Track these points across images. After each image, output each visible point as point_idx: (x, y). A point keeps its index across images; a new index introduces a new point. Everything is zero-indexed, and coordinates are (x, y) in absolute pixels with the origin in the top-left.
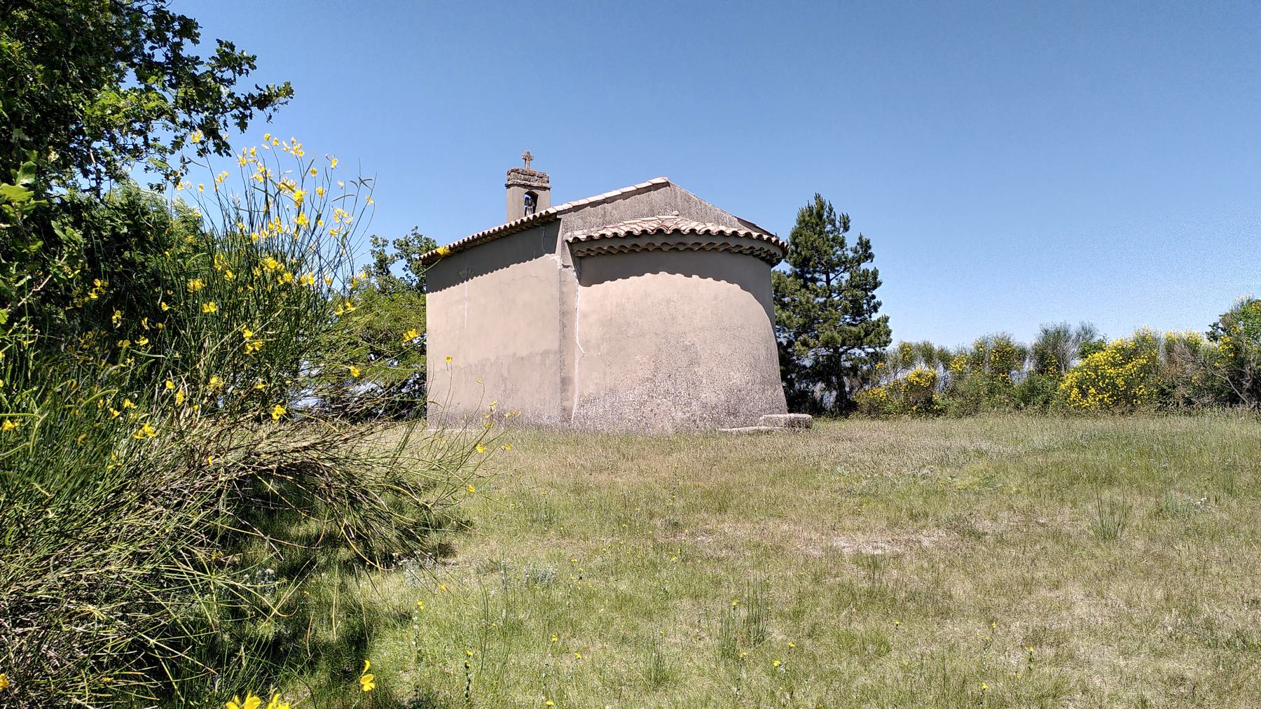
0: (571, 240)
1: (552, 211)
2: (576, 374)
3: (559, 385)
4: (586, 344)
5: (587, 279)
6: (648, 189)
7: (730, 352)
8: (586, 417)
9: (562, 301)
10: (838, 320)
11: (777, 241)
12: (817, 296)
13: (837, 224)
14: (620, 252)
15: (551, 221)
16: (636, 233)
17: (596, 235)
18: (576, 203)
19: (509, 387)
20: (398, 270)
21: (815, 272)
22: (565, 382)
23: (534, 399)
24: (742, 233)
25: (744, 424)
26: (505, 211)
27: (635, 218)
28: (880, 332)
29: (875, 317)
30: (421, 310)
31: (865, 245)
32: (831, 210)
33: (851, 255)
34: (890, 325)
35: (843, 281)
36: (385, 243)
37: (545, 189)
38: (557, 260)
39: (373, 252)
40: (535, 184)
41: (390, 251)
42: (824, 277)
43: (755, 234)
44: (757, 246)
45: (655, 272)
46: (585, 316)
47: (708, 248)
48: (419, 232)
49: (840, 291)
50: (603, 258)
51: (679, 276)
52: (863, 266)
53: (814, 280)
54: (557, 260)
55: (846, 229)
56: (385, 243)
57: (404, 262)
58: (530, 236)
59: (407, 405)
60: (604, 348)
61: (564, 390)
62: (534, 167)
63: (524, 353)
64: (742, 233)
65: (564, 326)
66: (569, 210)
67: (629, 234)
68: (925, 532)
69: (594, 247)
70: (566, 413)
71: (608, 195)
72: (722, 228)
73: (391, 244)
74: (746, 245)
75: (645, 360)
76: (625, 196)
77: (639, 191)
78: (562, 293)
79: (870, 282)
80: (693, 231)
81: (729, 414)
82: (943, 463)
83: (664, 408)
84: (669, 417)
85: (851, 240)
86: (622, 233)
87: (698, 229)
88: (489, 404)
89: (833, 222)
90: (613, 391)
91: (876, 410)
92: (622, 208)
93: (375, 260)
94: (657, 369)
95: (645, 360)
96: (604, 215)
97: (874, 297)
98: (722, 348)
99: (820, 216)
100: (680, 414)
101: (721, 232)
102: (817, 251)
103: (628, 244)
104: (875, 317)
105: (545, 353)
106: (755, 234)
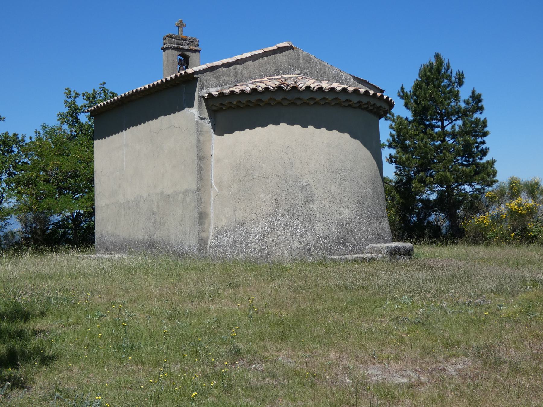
2: (212, 210)
4: (220, 184)
5: (220, 129)
6: (274, 52)
7: (340, 191)
9: (199, 148)
10: (450, 161)
11: (388, 98)
12: (433, 140)
13: (453, 79)
14: (248, 106)
15: (190, 81)
16: (260, 89)
17: (227, 92)
18: (210, 65)
19: (158, 220)
20: (84, 118)
21: (432, 119)
22: (202, 217)
23: (178, 230)
24: (362, 90)
25: (352, 252)
26: (160, 70)
27: (262, 77)
28: (486, 173)
29: (485, 160)
31: (476, 98)
32: (448, 68)
33: (463, 105)
34: (496, 166)
35: (457, 128)
36: (77, 95)
37: (195, 51)
38: (194, 113)
39: (66, 102)
41: (80, 102)
42: (439, 123)
43: (371, 92)
44: (365, 100)
45: (277, 123)
46: (218, 161)
47: (322, 102)
48: (106, 86)
49: (454, 135)
50: (234, 112)
51: (297, 127)
52: (476, 116)
53: (433, 127)
55: (460, 83)
56: (77, 95)
59: (80, 234)
60: (235, 187)
62: (186, 33)
63: (170, 192)
64: (362, 90)
65: (200, 169)
66: (205, 71)
67: (254, 90)
68: (453, 360)
69: (225, 102)
70: (203, 242)
71: (239, 57)
72: (335, 85)
73: (81, 97)
74: (355, 99)
75: (268, 198)
76: (254, 58)
77: (266, 54)
78: (199, 141)
79: (479, 130)
80: (308, 88)
81: (339, 244)
82: (499, 291)
84: (287, 245)
85: (464, 93)
86: (248, 90)
87: (312, 86)
88: (139, 234)
89: (449, 78)
90: (241, 224)
91: (480, 237)
92: (251, 68)
94: (278, 206)
95: (268, 198)
96: (236, 74)
97: (484, 143)
98: (334, 188)
99: (439, 71)
100: (297, 243)
101: (332, 89)
102: (435, 102)
104: (485, 160)
106: (371, 92)
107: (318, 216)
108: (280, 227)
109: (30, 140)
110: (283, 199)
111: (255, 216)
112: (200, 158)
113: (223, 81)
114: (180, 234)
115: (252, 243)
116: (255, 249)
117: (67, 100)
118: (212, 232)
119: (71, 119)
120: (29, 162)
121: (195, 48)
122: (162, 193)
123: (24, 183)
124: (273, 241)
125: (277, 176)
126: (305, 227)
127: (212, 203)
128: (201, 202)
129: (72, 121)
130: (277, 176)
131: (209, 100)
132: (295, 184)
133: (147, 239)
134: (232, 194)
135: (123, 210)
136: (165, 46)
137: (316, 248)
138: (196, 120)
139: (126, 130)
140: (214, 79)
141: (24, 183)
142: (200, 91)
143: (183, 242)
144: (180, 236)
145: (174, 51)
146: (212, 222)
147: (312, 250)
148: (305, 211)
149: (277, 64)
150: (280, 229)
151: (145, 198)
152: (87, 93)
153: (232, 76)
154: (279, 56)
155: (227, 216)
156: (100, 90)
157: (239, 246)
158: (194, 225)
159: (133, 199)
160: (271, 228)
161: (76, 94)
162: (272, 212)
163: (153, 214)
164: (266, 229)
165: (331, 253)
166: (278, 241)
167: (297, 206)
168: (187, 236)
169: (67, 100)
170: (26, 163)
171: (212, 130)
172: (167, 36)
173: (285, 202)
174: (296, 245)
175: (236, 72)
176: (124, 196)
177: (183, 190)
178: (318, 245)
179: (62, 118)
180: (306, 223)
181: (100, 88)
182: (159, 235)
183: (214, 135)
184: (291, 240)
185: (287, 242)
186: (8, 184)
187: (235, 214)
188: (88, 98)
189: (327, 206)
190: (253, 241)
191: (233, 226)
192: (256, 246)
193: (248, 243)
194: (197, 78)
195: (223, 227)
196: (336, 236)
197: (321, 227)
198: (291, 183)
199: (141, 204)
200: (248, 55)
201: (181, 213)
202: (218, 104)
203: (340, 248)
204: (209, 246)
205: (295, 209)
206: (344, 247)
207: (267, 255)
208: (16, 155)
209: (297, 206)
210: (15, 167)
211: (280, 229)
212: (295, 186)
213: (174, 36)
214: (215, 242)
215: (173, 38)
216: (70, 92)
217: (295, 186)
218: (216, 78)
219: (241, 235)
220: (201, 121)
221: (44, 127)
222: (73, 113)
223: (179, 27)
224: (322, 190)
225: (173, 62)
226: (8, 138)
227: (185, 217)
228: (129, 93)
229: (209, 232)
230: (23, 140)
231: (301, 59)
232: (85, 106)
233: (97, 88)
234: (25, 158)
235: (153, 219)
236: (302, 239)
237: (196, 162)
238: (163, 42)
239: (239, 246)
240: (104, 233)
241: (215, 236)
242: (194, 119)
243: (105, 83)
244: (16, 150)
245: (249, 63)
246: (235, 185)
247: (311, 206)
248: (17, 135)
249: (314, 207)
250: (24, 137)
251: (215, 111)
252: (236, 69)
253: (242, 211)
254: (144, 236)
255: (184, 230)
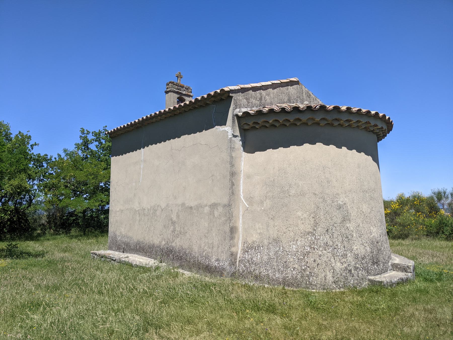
0: (240, 114)
1: (226, 89)
3: (228, 234)
4: (250, 200)
5: (250, 147)
8: (251, 261)
18: (242, 86)
19: (178, 229)
20: (93, 147)
22: (233, 230)
23: (200, 240)
30: (108, 167)
36: (88, 133)
38: (229, 129)
39: (81, 137)
40: (184, 93)
41: (90, 137)
46: (248, 177)
50: (267, 130)
51: (332, 147)
54: (229, 129)
56: (88, 133)
57: (97, 143)
58: (203, 113)
60: (268, 204)
61: (232, 238)
62: (180, 82)
71: (264, 84)
73: (91, 134)
75: (305, 215)
76: (274, 86)
81: (374, 263)
83: (324, 259)
88: (156, 239)
90: (277, 241)
93: (81, 141)
94: (316, 224)
96: (261, 99)
98: (365, 208)
100: (339, 264)
103: (291, 118)
105: (214, 206)
107: (355, 235)
108: (320, 247)
109: (55, 160)
110: (322, 217)
111: (292, 234)
112: (232, 174)
113: (252, 103)
114: (205, 246)
115: (290, 262)
116: (294, 268)
117: (82, 135)
118: (240, 246)
119: (83, 148)
120: (54, 173)
121: (189, 94)
122: (183, 204)
123: (49, 187)
124: (315, 261)
125: (315, 194)
126: (344, 247)
127: (241, 217)
128: (232, 216)
129: (84, 149)
130: (315, 194)
131: (243, 119)
132: (333, 202)
133: (165, 245)
134: (264, 210)
135: (138, 216)
136: (168, 90)
137: (356, 268)
138: (230, 137)
139: (144, 148)
140: (245, 100)
141: (49, 187)
142: (234, 110)
143: (210, 255)
144: (206, 248)
145: (175, 94)
146: (241, 236)
147: (353, 271)
148: (343, 231)
149: (289, 94)
150: (321, 249)
151: (163, 207)
152: (95, 132)
153: (258, 99)
154: (291, 89)
155: (259, 231)
156: (103, 131)
157: (275, 264)
158: (225, 239)
159: (149, 208)
160: (311, 248)
161: (88, 131)
162: (311, 230)
163: (172, 223)
164: (306, 248)
165: (369, 273)
166: (319, 261)
167: (336, 225)
168: (215, 249)
169: (82, 135)
170: (52, 174)
171: (242, 148)
172: (170, 83)
173: (323, 220)
174: (338, 266)
175: (261, 97)
176: (139, 204)
177: (209, 204)
178: (357, 266)
179: (78, 146)
180: (345, 243)
181: (104, 129)
182: (177, 244)
183: (244, 153)
184: (332, 260)
185: (329, 262)
186: (38, 187)
187: (268, 230)
188: (96, 135)
189: (361, 225)
190: (292, 260)
191: (266, 242)
192: (296, 266)
193: (286, 262)
194: (232, 97)
195: (253, 242)
196: (371, 255)
197: (358, 247)
198: (329, 201)
199: (158, 213)
200: (269, 83)
201: (206, 225)
202: (251, 123)
203: (375, 268)
204: (238, 261)
205: (334, 228)
206: (377, 266)
207: (308, 276)
208: (45, 169)
209: (336, 225)
210: (44, 176)
211: (321, 249)
212: (333, 204)
213: (175, 83)
214: (245, 258)
215: (174, 84)
216: (84, 130)
217: (333, 204)
218: (247, 99)
219: (276, 252)
220: (233, 139)
221: (65, 151)
222: (85, 143)
223: (178, 77)
224: (356, 210)
225: (174, 102)
226: (40, 157)
227: (211, 230)
228: (151, 115)
229: (238, 246)
230: (51, 159)
231: (304, 93)
232: (93, 140)
233: (101, 129)
234: (51, 171)
235: (172, 227)
236: (344, 260)
237: (228, 177)
238: (166, 87)
239: (275, 264)
240: (118, 233)
241: (245, 251)
242: (228, 136)
243: (106, 126)
244: (45, 165)
245: (270, 90)
246: (267, 201)
247: (348, 226)
248: (47, 155)
249: (351, 226)
250: (51, 157)
251: (245, 130)
252: (261, 94)
253: (276, 228)
254: (160, 242)
255: (210, 242)
